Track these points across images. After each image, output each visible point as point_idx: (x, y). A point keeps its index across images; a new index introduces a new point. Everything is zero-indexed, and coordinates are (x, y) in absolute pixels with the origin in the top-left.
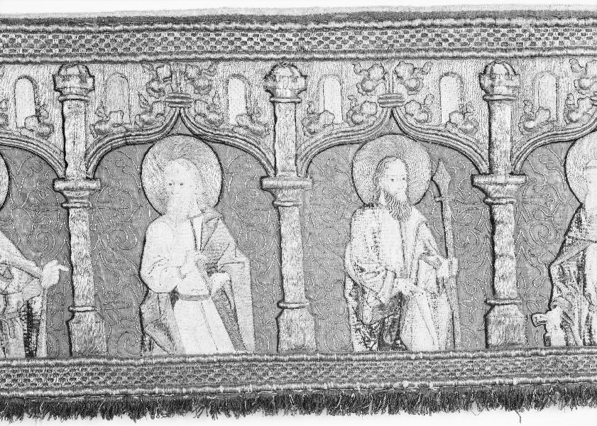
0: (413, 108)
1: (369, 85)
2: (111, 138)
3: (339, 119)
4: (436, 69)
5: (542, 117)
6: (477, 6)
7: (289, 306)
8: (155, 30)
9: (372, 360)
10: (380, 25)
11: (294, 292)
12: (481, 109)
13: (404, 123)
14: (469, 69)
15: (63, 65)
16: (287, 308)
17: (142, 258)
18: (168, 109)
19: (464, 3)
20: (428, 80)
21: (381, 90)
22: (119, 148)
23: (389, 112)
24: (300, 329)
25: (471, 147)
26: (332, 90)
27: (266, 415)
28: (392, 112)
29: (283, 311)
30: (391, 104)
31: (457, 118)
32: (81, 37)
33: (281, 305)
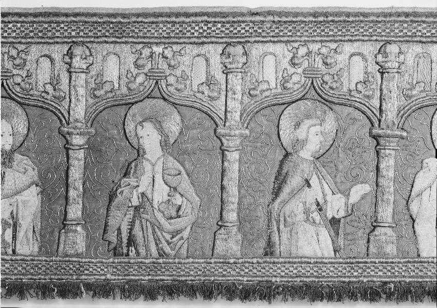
0: (171, 80)
1: (140, 62)
2: (417, 98)
3: (273, 85)
4: (348, 48)
5: (107, 87)
6: (123, 9)
7: (380, 224)
8: (39, 22)
9: (299, 263)
10: (188, 20)
11: (231, 216)
12: (221, 77)
13: (13, 93)
14: (58, 52)
15: (229, 44)
16: (379, 226)
17: (412, 187)
18: (303, 78)
19: (10, 6)
20: (186, 59)
21: (306, 64)
22: (114, 107)
23: (310, 82)
24: (230, 244)
25: (365, 105)
26: (271, 64)
27: (270, 303)
28: (312, 83)
29: (220, 228)
30: (156, 77)
31: (49, 88)
32: (366, 25)
33: (220, 223)
